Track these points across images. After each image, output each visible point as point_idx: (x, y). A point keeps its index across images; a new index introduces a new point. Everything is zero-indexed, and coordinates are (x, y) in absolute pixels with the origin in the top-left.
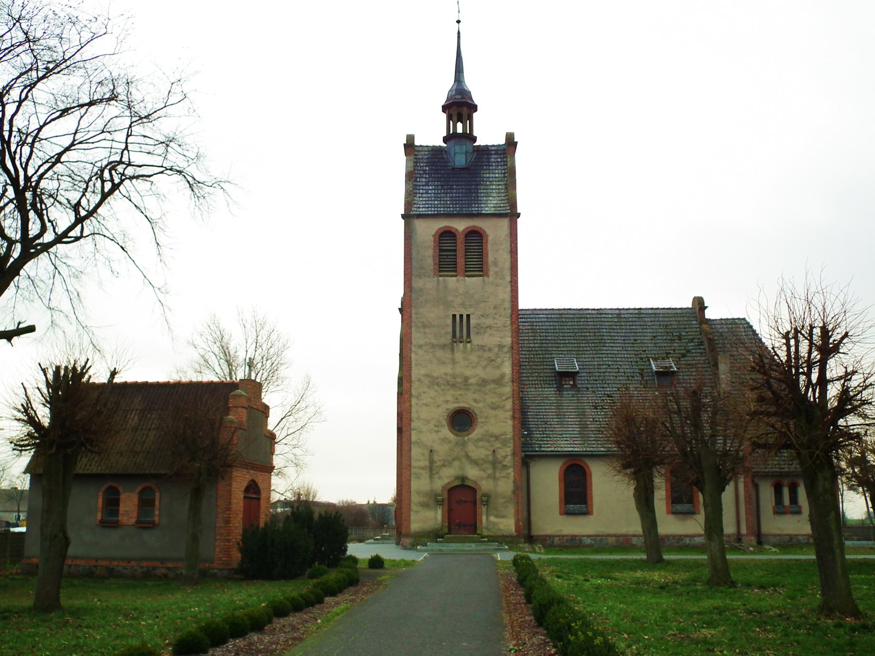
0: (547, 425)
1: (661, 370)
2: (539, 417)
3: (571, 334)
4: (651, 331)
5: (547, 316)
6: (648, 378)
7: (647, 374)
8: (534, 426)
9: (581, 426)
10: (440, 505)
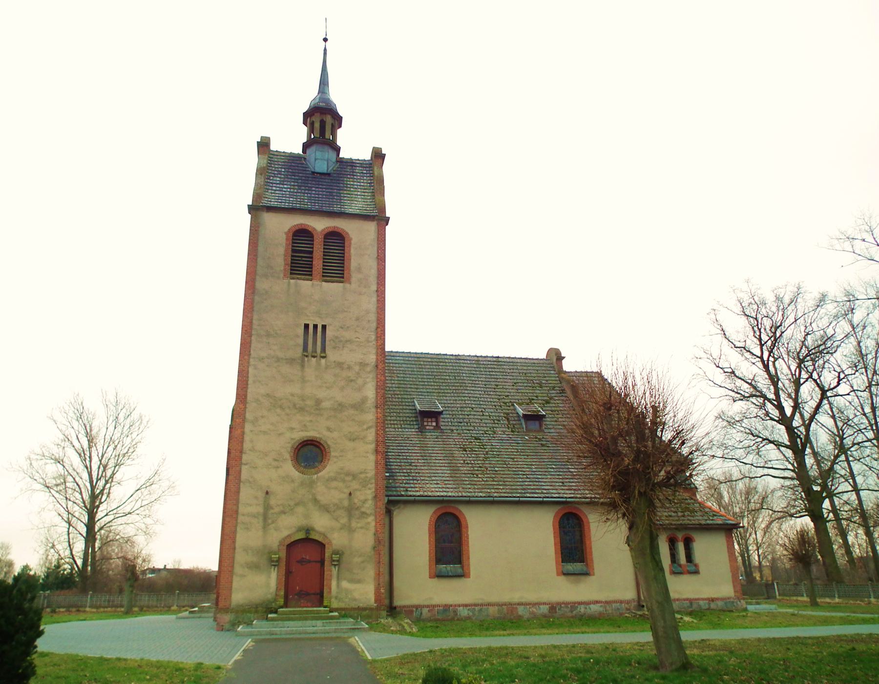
0: (412, 466)
1: (530, 413)
2: (401, 457)
3: (430, 377)
4: (511, 377)
5: (405, 358)
6: (514, 422)
7: (513, 419)
8: (397, 467)
9: (452, 468)
10: (275, 566)
